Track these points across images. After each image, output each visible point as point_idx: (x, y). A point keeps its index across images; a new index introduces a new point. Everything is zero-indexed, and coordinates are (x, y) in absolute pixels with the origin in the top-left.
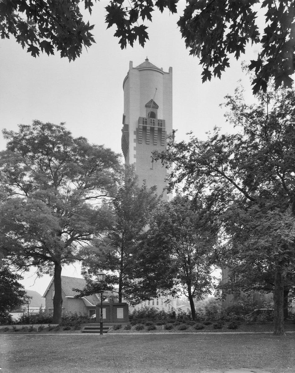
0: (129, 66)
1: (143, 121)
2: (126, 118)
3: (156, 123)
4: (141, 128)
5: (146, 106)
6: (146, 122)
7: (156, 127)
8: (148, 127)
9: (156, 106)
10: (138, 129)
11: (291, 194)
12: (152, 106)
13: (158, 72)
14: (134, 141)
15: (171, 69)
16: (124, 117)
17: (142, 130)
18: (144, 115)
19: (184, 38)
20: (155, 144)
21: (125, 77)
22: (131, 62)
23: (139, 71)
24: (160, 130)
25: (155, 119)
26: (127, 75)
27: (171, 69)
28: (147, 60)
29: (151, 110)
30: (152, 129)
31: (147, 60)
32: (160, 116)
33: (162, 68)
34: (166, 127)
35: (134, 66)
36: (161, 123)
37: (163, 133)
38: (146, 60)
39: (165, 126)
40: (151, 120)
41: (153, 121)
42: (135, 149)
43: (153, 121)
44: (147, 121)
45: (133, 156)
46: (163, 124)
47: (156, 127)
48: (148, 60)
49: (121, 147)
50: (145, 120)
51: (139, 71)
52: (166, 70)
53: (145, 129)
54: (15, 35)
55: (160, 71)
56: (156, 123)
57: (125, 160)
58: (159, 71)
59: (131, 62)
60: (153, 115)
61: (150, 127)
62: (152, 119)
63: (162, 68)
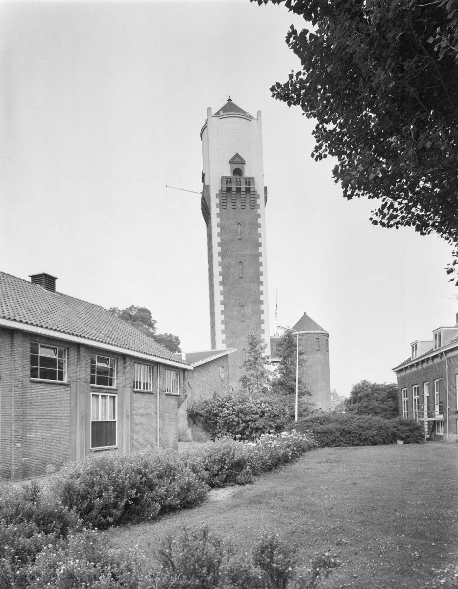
0: (301, 317)
1: (226, 180)
2: (206, 177)
3: (243, 181)
4: (225, 189)
5: (230, 162)
7: (243, 187)
8: (234, 187)
10: (221, 191)
12: (237, 164)
14: (221, 293)
15: (259, 113)
16: (203, 175)
17: (225, 193)
18: (228, 173)
19: (30, 278)
24: (248, 190)
25: (241, 177)
26: (205, 123)
27: (259, 113)
28: (230, 100)
29: (236, 166)
30: (239, 190)
31: (230, 100)
32: (247, 174)
36: (250, 181)
38: (228, 100)
39: (254, 185)
40: (236, 179)
41: (238, 180)
43: (238, 180)
45: (217, 235)
46: (252, 183)
47: (243, 187)
48: (231, 100)
49: (201, 211)
50: (229, 180)
51: (220, 119)
53: (229, 190)
54: (314, 151)
56: (243, 181)
57: (207, 226)
60: (238, 172)
61: (237, 187)
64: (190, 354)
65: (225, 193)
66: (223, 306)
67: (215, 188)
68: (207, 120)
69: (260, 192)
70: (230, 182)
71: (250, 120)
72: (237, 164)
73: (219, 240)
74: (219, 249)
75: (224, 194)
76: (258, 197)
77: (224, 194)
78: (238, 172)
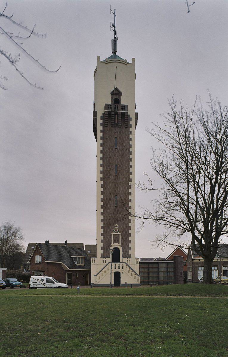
1: (107, 106)
6: (118, 108)
9: (120, 94)
11: (1, 330)
12: (116, 94)
13: (110, 63)
14: (131, 119)
15: (134, 60)
16: (94, 104)
17: (107, 115)
20: (119, 126)
21: (95, 69)
22: (99, 58)
23: (105, 64)
25: (119, 105)
26: (96, 68)
27: (134, 60)
29: (115, 97)
32: (123, 102)
33: (126, 60)
34: (128, 111)
35: (102, 60)
37: (126, 116)
40: (115, 106)
41: (116, 107)
42: (102, 131)
43: (116, 107)
44: (118, 107)
50: (110, 106)
51: (105, 64)
52: (130, 61)
55: (124, 63)
56: (120, 108)
58: (116, 61)
59: (99, 58)
60: (116, 101)
62: (115, 105)
63: (126, 60)
64: (97, 119)
65: (107, 115)
66: (102, 161)
67: (100, 114)
68: (17, 69)
69: (132, 116)
70: (111, 108)
71: (127, 65)
72: (116, 94)
73: (101, 128)
74: (101, 128)
75: (106, 122)
76: (131, 119)
77: (106, 122)
78: (116, 101)
